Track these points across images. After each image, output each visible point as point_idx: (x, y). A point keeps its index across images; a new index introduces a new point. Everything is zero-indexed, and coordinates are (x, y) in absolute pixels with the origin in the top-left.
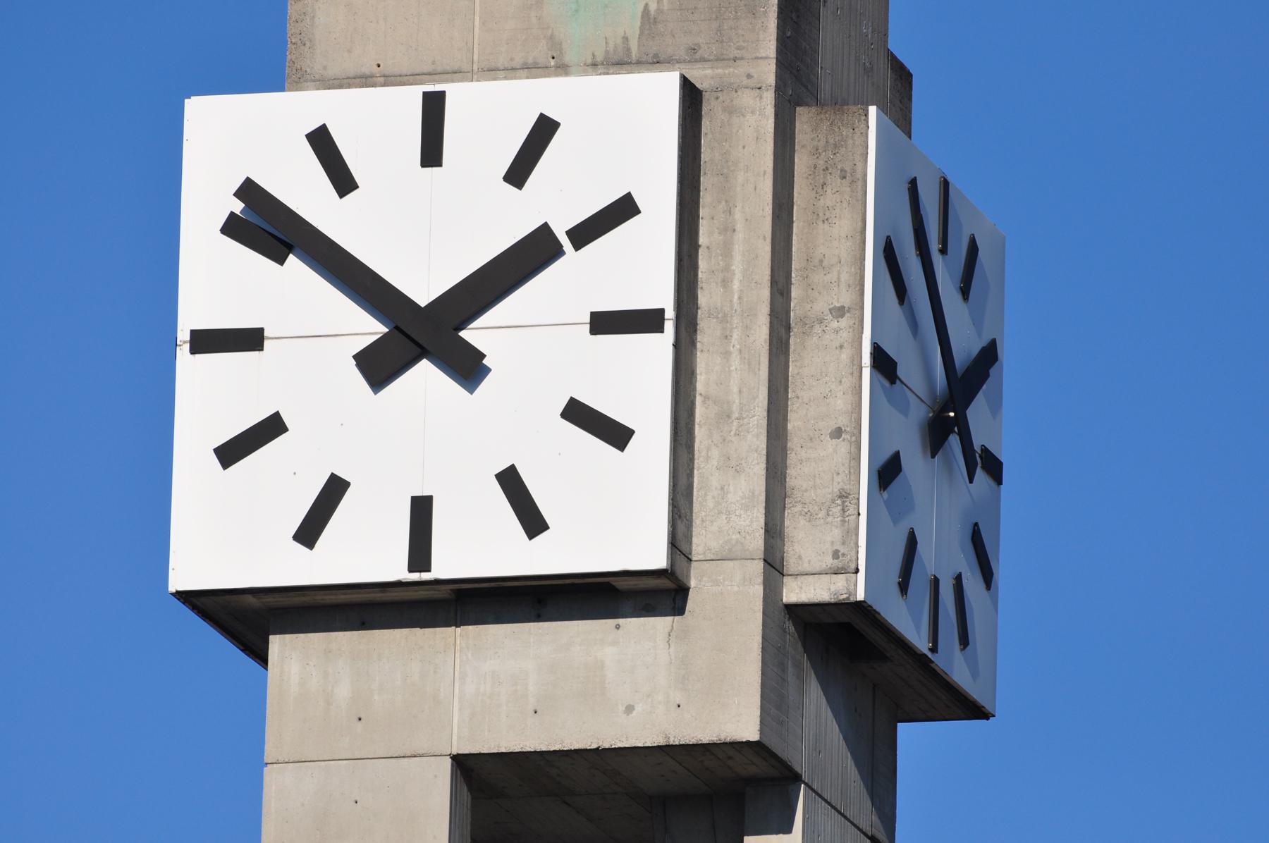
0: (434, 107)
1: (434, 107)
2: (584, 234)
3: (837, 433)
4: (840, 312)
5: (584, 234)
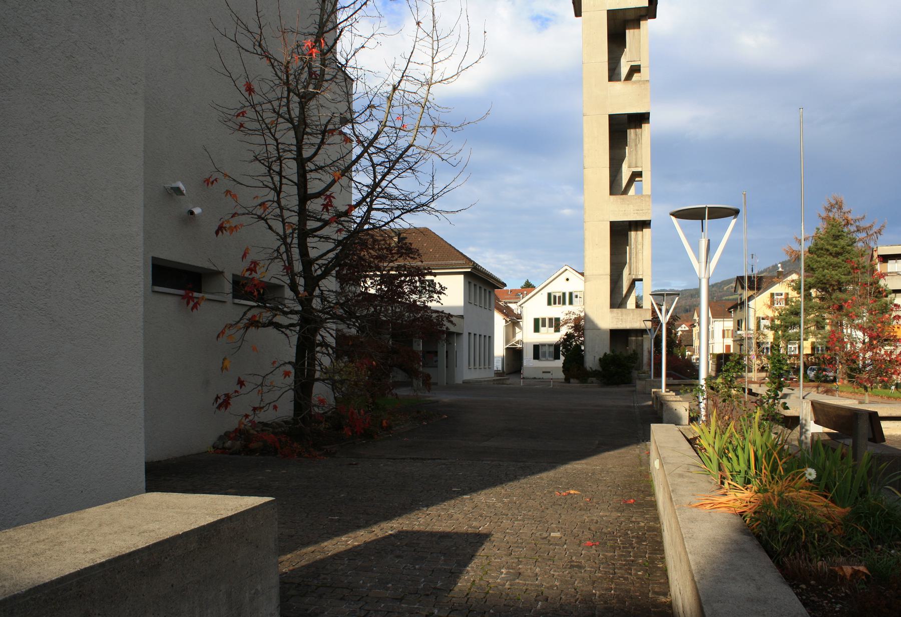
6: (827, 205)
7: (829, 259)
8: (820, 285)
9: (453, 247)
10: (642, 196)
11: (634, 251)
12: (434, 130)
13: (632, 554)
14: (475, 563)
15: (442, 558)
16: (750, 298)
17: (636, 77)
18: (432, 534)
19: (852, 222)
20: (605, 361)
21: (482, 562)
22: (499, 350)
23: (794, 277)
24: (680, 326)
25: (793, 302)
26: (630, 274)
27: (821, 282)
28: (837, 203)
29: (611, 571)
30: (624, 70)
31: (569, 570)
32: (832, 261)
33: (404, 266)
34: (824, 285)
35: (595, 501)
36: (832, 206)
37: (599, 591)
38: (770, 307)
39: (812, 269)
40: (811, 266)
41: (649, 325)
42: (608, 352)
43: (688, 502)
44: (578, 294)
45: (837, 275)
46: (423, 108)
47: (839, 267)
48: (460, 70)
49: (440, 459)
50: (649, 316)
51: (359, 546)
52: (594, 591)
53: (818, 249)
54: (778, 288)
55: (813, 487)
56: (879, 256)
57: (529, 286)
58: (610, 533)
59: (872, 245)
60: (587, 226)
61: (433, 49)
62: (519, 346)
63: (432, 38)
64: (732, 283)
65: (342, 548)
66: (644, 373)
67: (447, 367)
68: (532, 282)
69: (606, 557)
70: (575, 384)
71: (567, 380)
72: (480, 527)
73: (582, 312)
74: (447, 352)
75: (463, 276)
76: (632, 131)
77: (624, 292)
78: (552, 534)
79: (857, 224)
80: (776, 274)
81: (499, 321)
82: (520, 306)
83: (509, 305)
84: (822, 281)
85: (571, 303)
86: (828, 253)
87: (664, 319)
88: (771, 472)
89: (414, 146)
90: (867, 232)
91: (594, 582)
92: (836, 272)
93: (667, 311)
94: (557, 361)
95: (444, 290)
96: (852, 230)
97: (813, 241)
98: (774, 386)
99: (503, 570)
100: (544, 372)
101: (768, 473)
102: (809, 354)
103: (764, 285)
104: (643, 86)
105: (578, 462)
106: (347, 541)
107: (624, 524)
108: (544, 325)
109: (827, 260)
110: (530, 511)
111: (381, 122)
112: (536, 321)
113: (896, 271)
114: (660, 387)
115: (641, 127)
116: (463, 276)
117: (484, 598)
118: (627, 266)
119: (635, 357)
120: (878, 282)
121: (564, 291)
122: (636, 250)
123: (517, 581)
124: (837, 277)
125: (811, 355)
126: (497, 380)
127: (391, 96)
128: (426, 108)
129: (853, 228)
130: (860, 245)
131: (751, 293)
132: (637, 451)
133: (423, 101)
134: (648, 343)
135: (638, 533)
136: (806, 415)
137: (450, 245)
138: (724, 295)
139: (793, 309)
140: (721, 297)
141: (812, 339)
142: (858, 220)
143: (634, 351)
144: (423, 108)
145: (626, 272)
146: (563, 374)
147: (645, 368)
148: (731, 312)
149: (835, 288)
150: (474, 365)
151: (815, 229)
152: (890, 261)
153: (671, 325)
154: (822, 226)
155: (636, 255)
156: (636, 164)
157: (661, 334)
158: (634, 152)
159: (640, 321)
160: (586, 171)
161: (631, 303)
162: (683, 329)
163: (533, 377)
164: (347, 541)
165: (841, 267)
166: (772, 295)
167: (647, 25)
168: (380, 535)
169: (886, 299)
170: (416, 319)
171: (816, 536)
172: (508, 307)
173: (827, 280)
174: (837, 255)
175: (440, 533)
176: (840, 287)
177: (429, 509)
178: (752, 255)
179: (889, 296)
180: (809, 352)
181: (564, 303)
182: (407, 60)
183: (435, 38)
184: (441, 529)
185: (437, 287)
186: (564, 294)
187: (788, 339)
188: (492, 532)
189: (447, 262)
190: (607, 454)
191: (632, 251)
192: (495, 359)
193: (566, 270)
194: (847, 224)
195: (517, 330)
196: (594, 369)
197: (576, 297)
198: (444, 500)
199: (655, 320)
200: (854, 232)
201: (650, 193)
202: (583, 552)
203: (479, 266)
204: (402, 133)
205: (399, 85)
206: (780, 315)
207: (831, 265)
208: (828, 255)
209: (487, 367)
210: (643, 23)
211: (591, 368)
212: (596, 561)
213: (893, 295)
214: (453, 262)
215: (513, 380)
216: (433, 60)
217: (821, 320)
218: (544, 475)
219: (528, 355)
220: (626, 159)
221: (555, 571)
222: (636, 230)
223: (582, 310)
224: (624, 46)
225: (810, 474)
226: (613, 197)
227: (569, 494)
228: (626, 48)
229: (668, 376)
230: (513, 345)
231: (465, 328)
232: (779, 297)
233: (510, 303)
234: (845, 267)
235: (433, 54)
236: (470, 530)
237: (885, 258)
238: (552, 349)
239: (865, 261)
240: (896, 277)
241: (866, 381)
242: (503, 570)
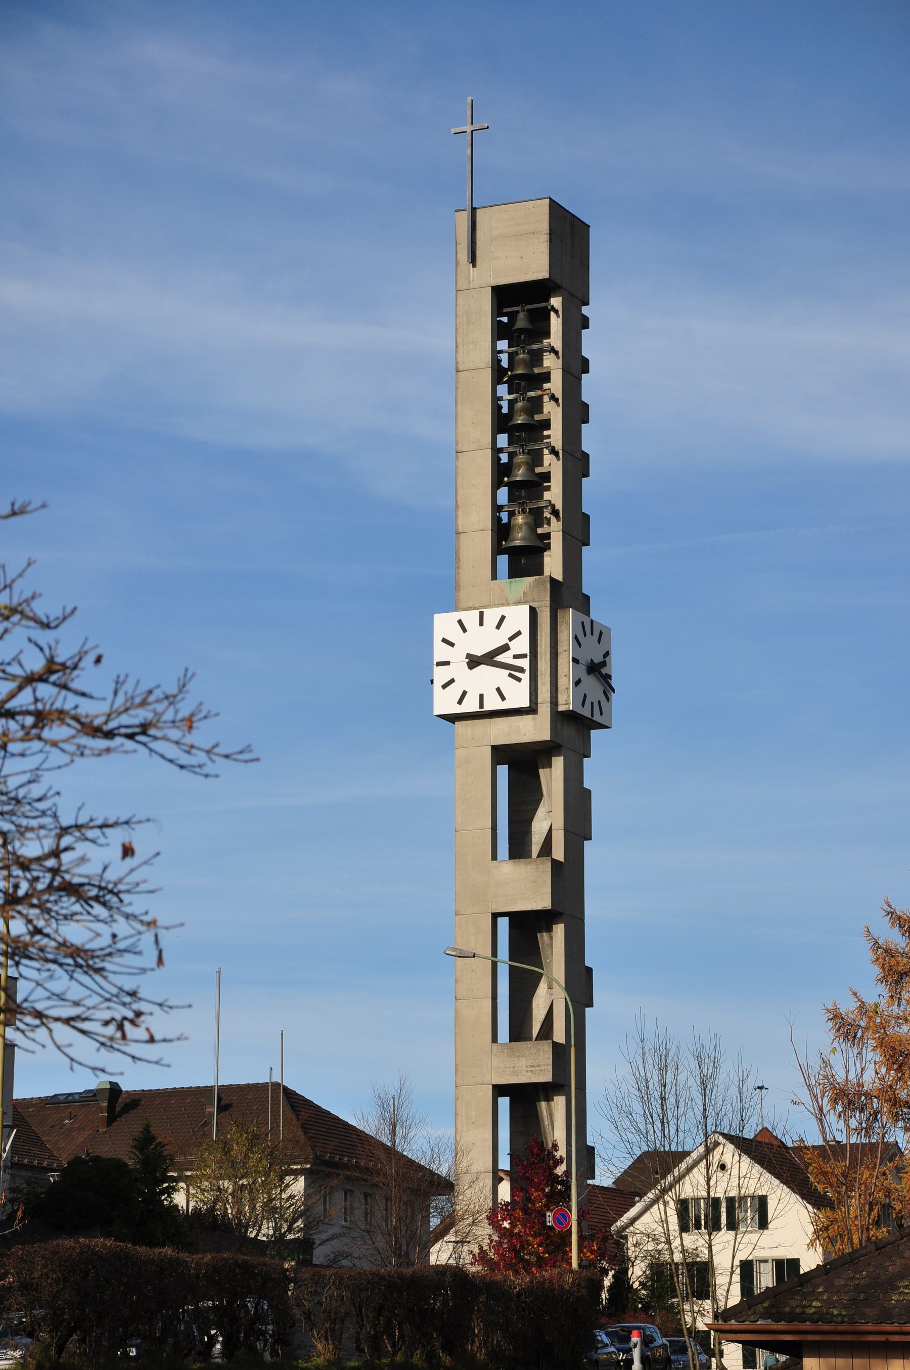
3: (566, 676)
4: (565, 651)
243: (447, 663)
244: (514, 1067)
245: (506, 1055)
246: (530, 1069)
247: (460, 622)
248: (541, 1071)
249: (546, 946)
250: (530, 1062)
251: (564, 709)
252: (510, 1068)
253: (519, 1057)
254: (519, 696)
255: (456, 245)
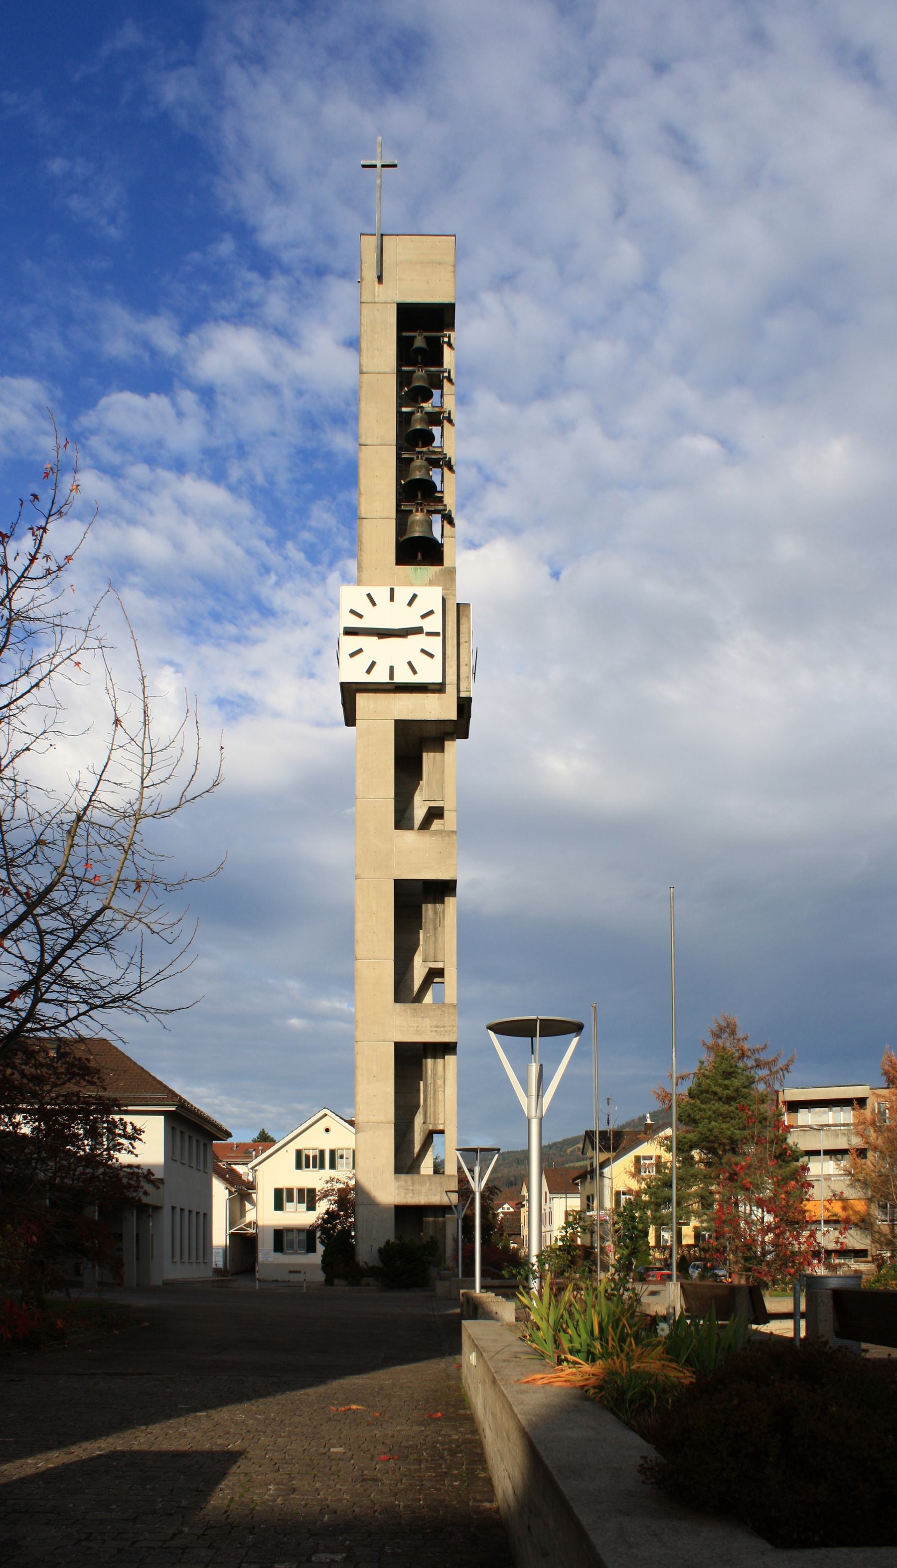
0: (392, 590)
1: (392, 590)
2: (428, 634)
3: (466, 665)
4: (466, 642)
5: (428, 634)
6: (714, 1027)
7: (718, 1105)
8: (705, 1143)
9: (146, 1072)
10: (444, 1005)
11: (431, 1089)
12: (138, 887)
13: (443, 1466)
14: (229, 1481)
15: (182, 1477)
16: (603, 1165)
17: (436, 825)
18: (161, 1454)
19: (749, 1054)
20: (386, 1252)
21: (239, 1481)
22: (220, 1236)
23: (668, 1132)
24: (501, 1206)
25: (667, 1168)
26: (424, 1123)
27: (706, 1139)
28: (728, 1026)
29: (418, 1483)
30: (419, 813)
31: (361, 1484)
32: (722, 1109)
33: (77, 1094)
34: (709, 1144)
35: (387, 1415)
36: (721, 1029)
37: (403, 1502)
38: (634, 1176)
39: (695, 1121)
40: (692, 1115)
41: (454, 1198)
42: (392, 1239)
43: (516, 1379)
44: (344, 1152)
45: (728, 1129)
46: (126, 852)
47: (731, 1118)
48: (184, 800)
49: (150, 1374)
50: (454, 1185)
51: (56, 1468)
52: (397, 1502)
53: (702, 1092)
54: (649, 1149)
55: (671, 1359)
56: (785, 1103)
57: (265, 1140)
58: (412, 1446)
59: (777, 1087)
60: (359, 1047)
61: (143, 765)
62: (251, 1231)
63: (142, 749)
64: (578, 1143)
65: (30, 1471)
66: (448, 1269)
67: (138, 1259)
68: (271, 1134)
69: (409, 1470)
70: (341, 1286)
71: (329, 1281)
72: (229, 1445)
73: (351, 1179)
74: (137, 1235)
75: (163, 1117)
76: (430, 906)
77: (416, 1150)
78: (332, 1450)
79: (757, 1056)
80: (643, 1129)
81: (220, 1192)
82: (252, 1168)
83: (234, 1166)
84: (708, 1137)
85: (333, 1166)
86: (716, 1098)
87: (477, 1186)
88: (619, 1342)
89: (111, 908)
90: (770, 1069)
91: (396, 1494)
92: (728, 1125)
93: (481, 1177)
94: (311, 1255)
95: (140, 1134)
96: (750, 1065)
97: (695, 1079)
98: (626, 1252)
99: (271, 1487)
100: (290, 1272)
101: (616, 1344)
102: (691, 1245)
103: (624, 1143)
104: (447, 839)
105: (358, 1376)
106: (36, 1464)
107: (430, 1437)
108: (290, 1200)
109: (714, 1108)
110: (296, 1427)
111: (56, 868)
112: (278, 1193)
113: (810, 1124)
114: (474, 1287)
115: (443, 902)
116: (163, 1117)
117: (250, 1514)
118: (421, 1110)
119: (434, 1247)
120: (785, 1139)
121: (322, 1148)
122: (434, 1086)
123: (292, 1496)
124: (729, 1133)
125: (694, 1246)
126: (218, 1281)
127: (73, 830)
128: (130, 852)
129: (750, 1063)
130: (761, 1087)
131: (604, 1156)
132: (443, 1365)
133: (126, 844)
134: (453, 1226)
135: (451, 1446)
136: (673, 1301)
137: (142, 1069)
138: (567, 1161)
139: (666, 1178)
140: (563, 1163)
141: (694, 1222)
142: (758, 1050)
143: (431, 1237)
144: (126, 852)
145: (418, 1120)
146: (321, 1272)
147: (449, 1263)
148: (577, 1184)
149: (727, 1148)
150: (181, 1258)
151: (698, 1063)
152: (801, 1110)
153: (490, 1193)
154: (708, 1058)
155: (434, 1094)
156: (435, 957)
157: (474, 1214)
158: (432, 939)
159: (441, 1192)
160: (358, 964)
161: (427, 1167)
162: (506, 1211)
163: (275, 1279)
164: (36, 1464)
165: (735, 1118)
166: (638, 1159)
167: (454, 747)
168: (84, 1456)
169: (796, 1163)
170: (93, 1178)
171: (670, 1400)
172: (233, 1170)
173: (716, 1137)
174: (729, 1100)
175: (172, 1452)
176: (734, 1146)
177: (150, 1427)
178: (608, 1099)
179: (801, 1160)
180: (691, 1241)
181: (322, 1167)
182: (98, 777)
183: (147, 749)
184: (173, 1448)
185: (129, 1129)
186: (322, 1152)
187: (659, 1221)
188: (248, 1450)
189: (137, 1095)
190: (398, 1368)
191: (429, 1089)
192: (214, 1251)
193: (325, 1115)
194: (743, 1056)
195: (248, 1206)
196: (371, 1265)
197: (342, 1157)
198: (169, 1417)
199: (465, 1191)
200: (752, 1068)
201: (455, 1002)
202: (377, 1466)
203: (189, 1103)
204: (85, 886)
205: (84, 814)
206: (649, 1187)
207: (721, 1114)
208: (716, 1100)
209: (201, 1260)
210: (448, 744)
211: (365, 1263)
212: (396, 1474)
213: (806, 1158)
214: (148, 1095)
215: (242, 1284)
216: (142, 783)
217: (707, 1194)
218: (310, 1390)
219: (266, 1246)
220: (421, 948)
221: (342, 1485)
222: (435, 1057)
223: (351, 1175)
224: (420, 777)
225: (662, 1330)
226: (398, 1005)
227: (349, 1409)
228: (421, 779)
229: (483, 1275)
230: (241, 1229)
231: (167, 1198)
232: (647, 1162)
233: (236, 1164)
234: (739, 1119)
235: (143, 773)
236: (215, 1448)
237: (794, 1106)
238: (304, 1237)
239: (767, 1108)
240: (808, 1133)
241: (765, 1275)
242: (271, 1487)
243: (392, 599)
244: (417, 1027)
245: (409, 1014)
246: (434, 1029)
247: (369, 596)
248: (446, 1031)
249: (429, 920)
250: (434, 1023)
251: (465, 696)
252: (413, 1027)
253: (423, 1017)
254: (430, 673)
255: (361, 263)
